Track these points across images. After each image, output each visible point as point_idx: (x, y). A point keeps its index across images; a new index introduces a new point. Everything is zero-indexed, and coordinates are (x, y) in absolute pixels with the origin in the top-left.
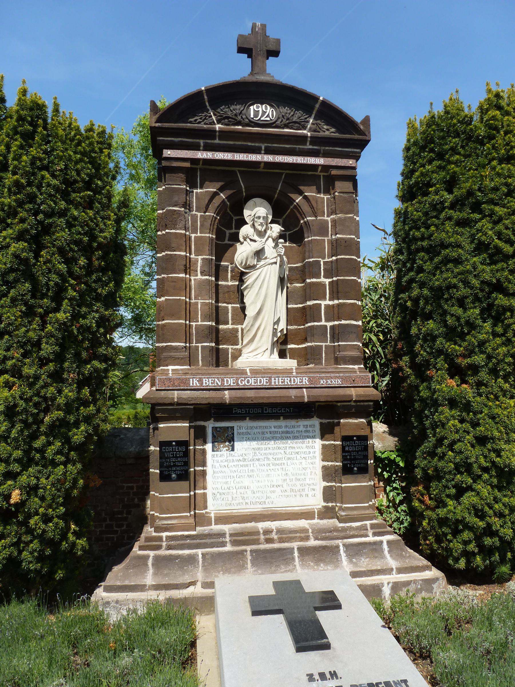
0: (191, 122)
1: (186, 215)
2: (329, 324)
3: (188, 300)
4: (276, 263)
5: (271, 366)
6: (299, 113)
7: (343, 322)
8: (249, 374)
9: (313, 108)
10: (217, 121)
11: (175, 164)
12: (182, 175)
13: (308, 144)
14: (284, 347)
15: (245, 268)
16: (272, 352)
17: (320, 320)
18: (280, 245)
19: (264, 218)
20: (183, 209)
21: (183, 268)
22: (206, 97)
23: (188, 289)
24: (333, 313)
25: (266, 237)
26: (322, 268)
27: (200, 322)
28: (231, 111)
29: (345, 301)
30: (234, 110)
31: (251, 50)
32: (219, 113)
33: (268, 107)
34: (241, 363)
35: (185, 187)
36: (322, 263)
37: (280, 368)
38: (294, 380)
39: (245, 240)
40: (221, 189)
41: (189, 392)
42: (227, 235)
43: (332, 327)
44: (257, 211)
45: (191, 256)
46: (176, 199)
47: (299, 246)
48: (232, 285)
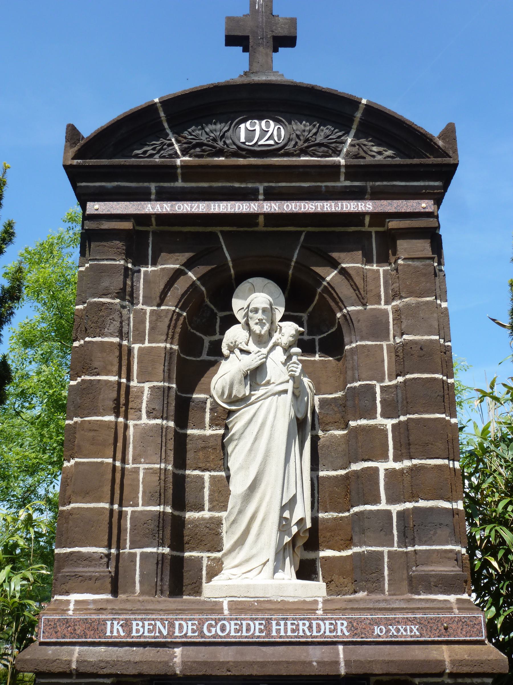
0: (137, 156)
1: (125, 312)
2: (395, 508)
3: (118, 464)
4: (285, 392)
5: (273, 595)
6: (326, 130)
7: (422, 504)
8: (226, 612)
9: (351, 121)
10: (181, 151)
11: (106, 225)
12: (118, 243)
13: (342, 178)
14: (311, 555)
15: (230, 403)
16: (278, 567)
17: (377, 500)
18: (294, 359)
19: (264, 310)
20: (118, 301)
21: (111, 404)
22: (162, 114)
23: (120, 444)
24: (402, 486)
25: (271, 344)
26: (378, 399)
27: (141, 507)
28: (207, 134)
29: (423, 462)
30: (212, 131)
31: (247, 38)
32: (185, 138)
33: (272, 123)
34: (212, 589)
35: (122, 262)
36: (378, 390)
37: (291, 600)
38: (318, 626)
39: (232, 352)
40: (190, 265)
41: (103, 649)
42: (206, 344)
43: (401, 514)
44: (256, 299)
45: (132, 384)
46: (105, 283)
47: (339, 360)
48: (212, 436)
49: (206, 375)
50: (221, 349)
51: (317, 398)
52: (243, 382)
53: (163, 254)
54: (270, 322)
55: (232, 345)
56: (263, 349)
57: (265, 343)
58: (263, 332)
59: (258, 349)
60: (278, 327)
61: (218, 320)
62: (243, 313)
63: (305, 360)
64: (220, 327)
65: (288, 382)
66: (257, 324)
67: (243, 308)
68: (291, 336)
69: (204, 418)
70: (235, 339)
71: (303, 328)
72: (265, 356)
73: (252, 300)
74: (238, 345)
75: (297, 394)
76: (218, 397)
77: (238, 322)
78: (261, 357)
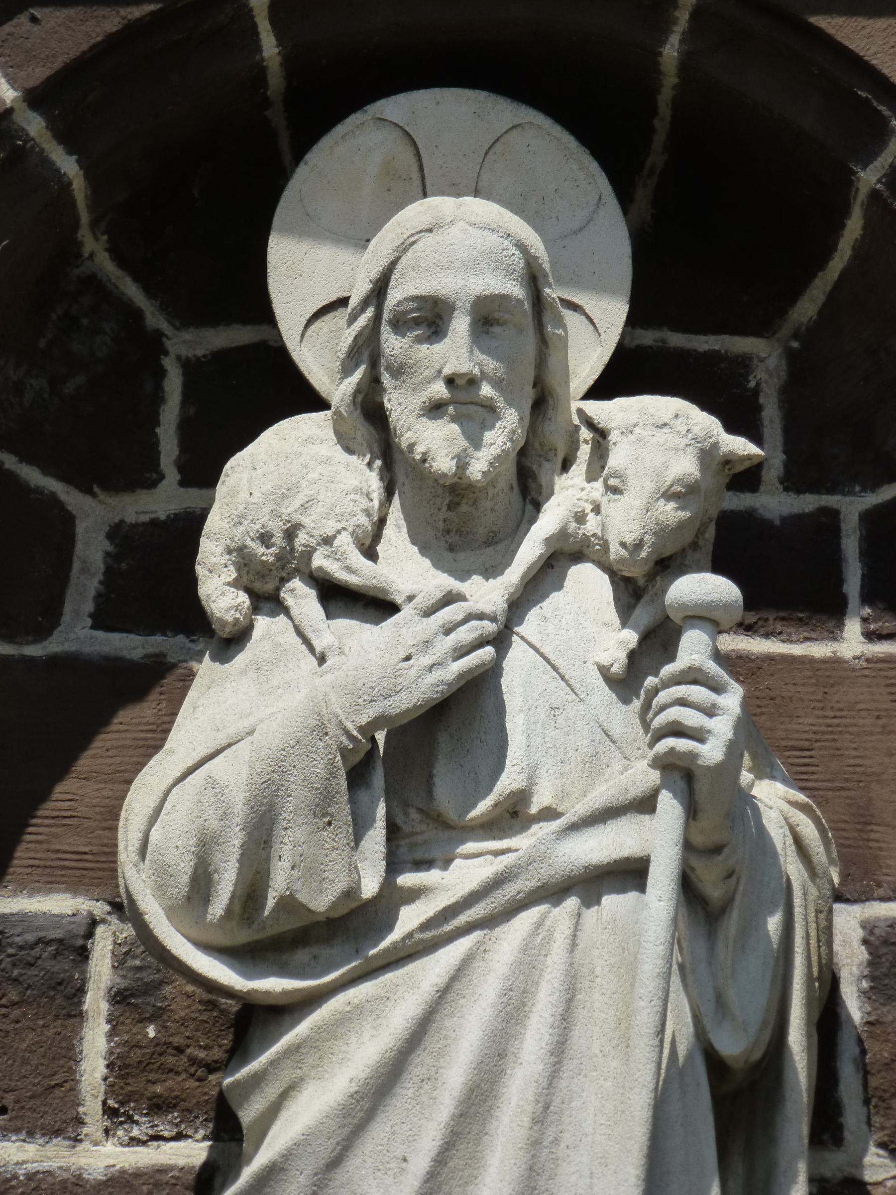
4: (631, 874)
15: (244, 955)
18: (693, 649)
19: (488, 317)
25: (530, 550)
39: (267, 601)
42: (91, 550)
49: (85, 762)
50: (193, 581)
51: (849, 921)
52: (342, 809)
53: (474, 577)
54: (528, 395)
55: (266, 554)
56: (477, 579)
57: (491, 541)
58: (478, 467)
59: (442, 581)
60: (585, 434)
61: (174, 384)
62: (342, 332)
63: (770, 659)
64: (187, 429)
65: (645, 804)
66: (435, 409)
67: (343, 302)
68: (668, 496)
69: (68, 1056)
70: (290, 509)
71: (756, 438)
72: (490, 627)
73: (405, 247)
74: (308, 554)
75: (714, 891)
76: (171, 912)
77: (311, 401)
78: (466, 634)
